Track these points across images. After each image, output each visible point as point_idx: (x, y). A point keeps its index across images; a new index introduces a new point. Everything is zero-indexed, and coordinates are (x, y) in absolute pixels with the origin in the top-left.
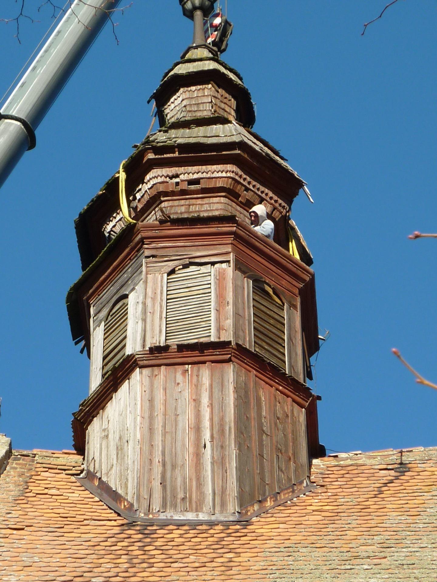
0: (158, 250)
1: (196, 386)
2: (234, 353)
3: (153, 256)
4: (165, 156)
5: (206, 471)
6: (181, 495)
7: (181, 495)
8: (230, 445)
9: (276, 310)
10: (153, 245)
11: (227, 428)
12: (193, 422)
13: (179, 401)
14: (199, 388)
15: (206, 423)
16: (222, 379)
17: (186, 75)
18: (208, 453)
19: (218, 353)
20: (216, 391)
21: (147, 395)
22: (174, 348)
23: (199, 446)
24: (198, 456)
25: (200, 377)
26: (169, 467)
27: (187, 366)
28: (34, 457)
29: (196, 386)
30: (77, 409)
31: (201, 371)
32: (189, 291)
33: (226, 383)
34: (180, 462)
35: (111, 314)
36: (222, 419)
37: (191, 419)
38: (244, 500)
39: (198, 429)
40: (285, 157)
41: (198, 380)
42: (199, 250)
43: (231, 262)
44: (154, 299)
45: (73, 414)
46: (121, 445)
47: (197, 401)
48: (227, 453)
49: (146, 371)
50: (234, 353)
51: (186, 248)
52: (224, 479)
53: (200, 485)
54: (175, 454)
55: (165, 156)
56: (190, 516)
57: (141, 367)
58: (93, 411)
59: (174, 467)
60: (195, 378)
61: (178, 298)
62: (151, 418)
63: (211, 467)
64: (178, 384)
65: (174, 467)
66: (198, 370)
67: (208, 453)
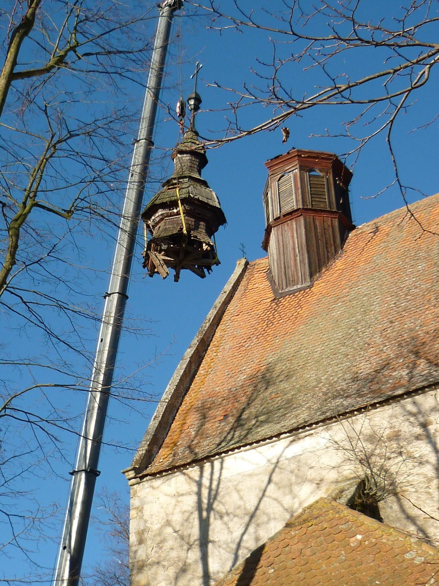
15: (297, 246)
18: (298, 258)
20: (299, 231)
23: (295, 256)
24: (295, 260)
36: (301, 242)
38: (311, 276)
47: (293, 236)
49: (275, 228)
65: (288, 268)
67: (298, 258)
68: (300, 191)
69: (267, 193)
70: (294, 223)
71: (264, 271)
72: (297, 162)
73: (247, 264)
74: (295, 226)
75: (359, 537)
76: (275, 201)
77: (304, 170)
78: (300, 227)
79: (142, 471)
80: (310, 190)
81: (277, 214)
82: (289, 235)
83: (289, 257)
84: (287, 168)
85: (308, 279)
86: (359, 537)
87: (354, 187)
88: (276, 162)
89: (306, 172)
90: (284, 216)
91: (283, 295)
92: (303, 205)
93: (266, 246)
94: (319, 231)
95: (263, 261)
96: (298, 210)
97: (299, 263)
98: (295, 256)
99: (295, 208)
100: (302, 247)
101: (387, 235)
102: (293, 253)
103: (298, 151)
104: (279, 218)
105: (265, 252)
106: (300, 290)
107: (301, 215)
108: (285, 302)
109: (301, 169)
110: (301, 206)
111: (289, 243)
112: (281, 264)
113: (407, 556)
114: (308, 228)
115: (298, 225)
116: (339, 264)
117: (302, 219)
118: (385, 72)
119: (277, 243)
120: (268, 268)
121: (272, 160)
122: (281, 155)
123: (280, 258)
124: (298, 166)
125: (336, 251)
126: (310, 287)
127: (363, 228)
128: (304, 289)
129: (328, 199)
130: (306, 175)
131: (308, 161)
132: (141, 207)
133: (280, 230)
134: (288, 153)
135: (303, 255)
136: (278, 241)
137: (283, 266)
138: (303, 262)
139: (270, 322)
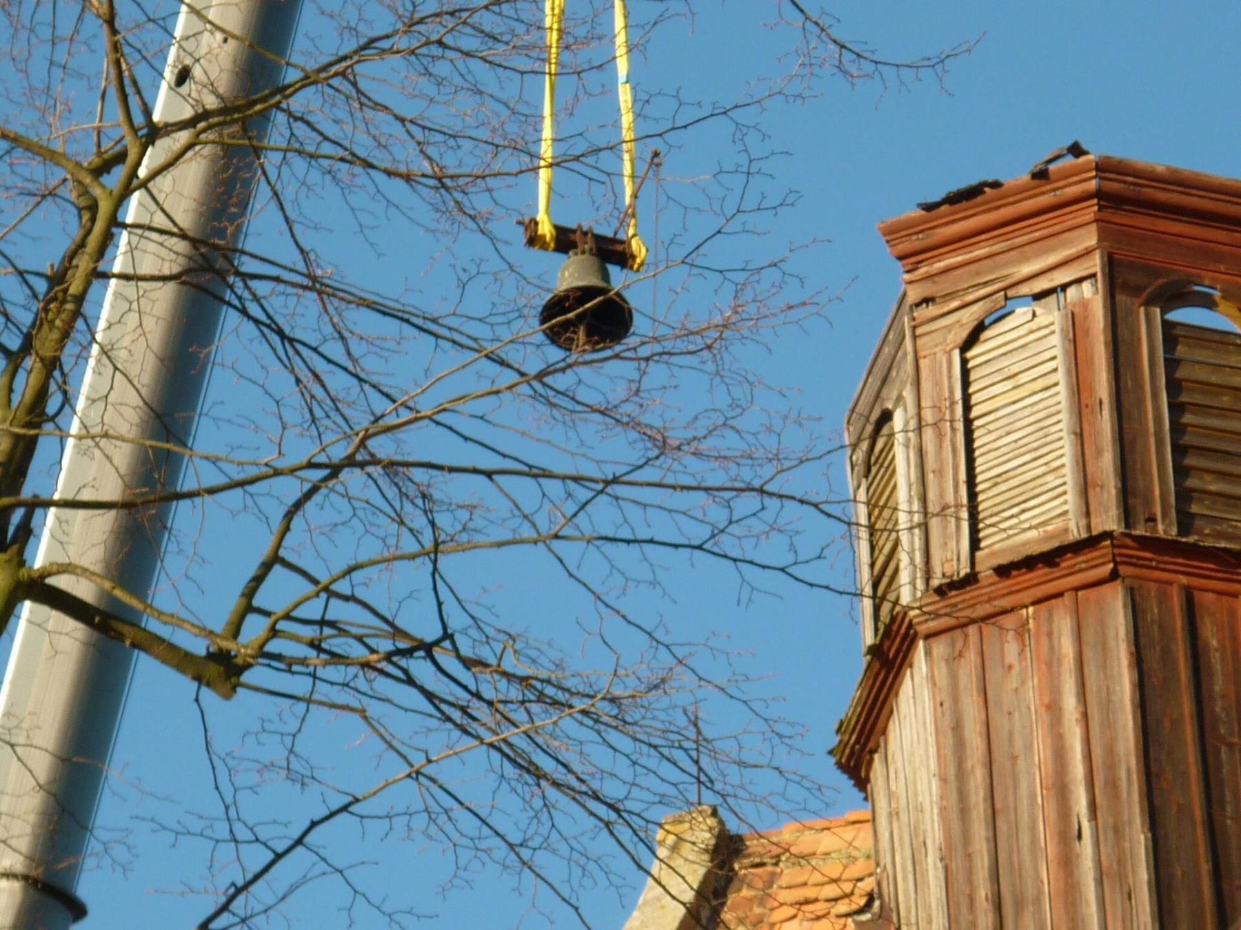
0: (936, 279)
1: (1049, 665)
2: (1121, 555)
3: (928, 300)
5: (1087, 903)
8: (1130, 823)
10: (923, 271)
11: (1123, 774)
12: (1050, 770)
13: (1016, 714)
14: (1055, 669)
15: (1078, 769)
16: (1104, 633)
18: (1086, 849)
19: (1083, 566)
20: (1091, 671)
21: (947, 714)
22: (987, 577)
23: (1067, 836)
24: (1068, 862)
25: (1055, 635)
26: (1008, 910)
27: (1024, 611)
28: (776, 864)
29: (1049, 665)
30: (834, 740)
31: (1056, 619)
32: (1014, 388)
33: (1111, 643)
34: (1030, 892)
35: (873, 459)
36: (1110, 751)
37: (1045, 763)
40: (716, 690)
41: (1052, 648)
42: (1026, 259)
43: (1099, 276)
45: (831, 752)
47: (1054, 708)
48: (1127, 845)
49: (940, 647)
50: (1121, 555)
51: (997, 258)
54: (1020, 869)
57: (928, 637)
58: (868, 740)
60: (1044, 641)
61: (997, 410)
63: (1097, 891)
64: (1010, 667)
65: (1019, 905)
66: (1050, 620)
67: (1086, 849)
68: (1105, 422)
69: (886, 416)
70: (1064, 626)
71: (843, 907)
72: (1090, 238)
73: (727, 849)
74: (1067, 647)
76: (940, 472)
77: (1135, 291)
78: (1104, 650)
81: (952, 556)
82: (1032, 696)
83: (1025, 839)
84: (1027, 269)
88: (960, 222)
89: (1148, 303)
90: (1003, 571)
92: (1128, 515)
93: (858, 752)
94: (1218, 687)
95: (827, 842)
96: (1090, 543)
98: (1067, 836)
99: (1076, 532)
100: (1113, 784)
102: (1052, 815)
103: (1104, 168)
104: (971, 579)
105: (845, 783)
107: (1114, 576)
109: (1119, 279)
110: (1108, 520)
111: (1029, 747)
112: (970, 881)
114: (1153, 658)
115: (1089, 637)
117: (1115, 602)
118: (872, 357)
119: (949, 741)
120: (868, 884)
121: (929, 207)
122: (996, 185)
123: (966, 840)
124: (1095, 264)
130: (1147, 327)
132: (700, 893)
133: (972, 656)
134: (1041, 175)
135: (1117, 831)
136: (957, 728)
137: (983, 891)
138: (1121, 877)
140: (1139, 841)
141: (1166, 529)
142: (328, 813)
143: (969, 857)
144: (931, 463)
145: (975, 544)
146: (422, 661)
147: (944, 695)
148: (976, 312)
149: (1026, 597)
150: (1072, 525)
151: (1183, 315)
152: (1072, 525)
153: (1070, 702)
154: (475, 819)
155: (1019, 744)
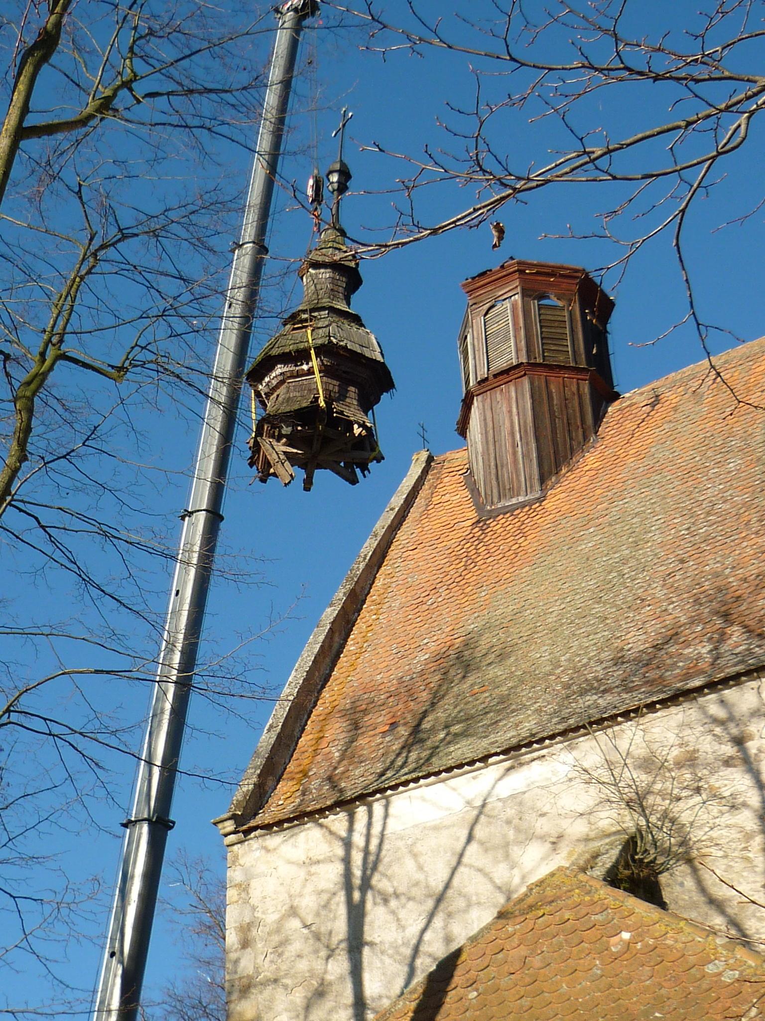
3: (475, 304)
4: (295, 451)
6: (508, 487)
7: (508, 487)
9: (558, 313)
15: (517, 428)
17: (441, 999)
20: (520, 402)
23: (514, 446)
24: (515, 453)
26: (499, 468)
34: (505, 462)
36: (525, 422)
38: (543, 480)
39: (512, 434)
44: (478, 339)
46: (477, 734)
47: (510, 412)
49: (480, 398)
52: (531, 467)
53: (518, 476)
55: (295, 451)
56: (514, 501)
57: (477, 395)
59: (502, 466)
62: (486, 433)
65: (502, 466)
68: (522, 332)
70: (513, 389)
72: (517, 283)
73: (430, 459)
74: (513, 394)
75: (626, 936)
76: (479, 350)
77: (530, 296)
78: (523, 395)
79: (248, 820)
80: (541, 332)
81: (483, 373)
83: (504, 449)
85: (537, 487)
86: (626, 936)
87: (616, 325)
89: (534, 299)
90: (495, 376)
91: (494, 515)
92: (529, 357)
93: (463, 428)
94: (555, 402)
95: (458, 455)
97: (522, 460)
100: (526, 431)
101: (675, 409)
102: (510, 441)
104: (487, 379)
106: (523, 505)
107: (525, 374)
108: (494, 526)
109: (525, 294)
112: (489, 461)
113: (710, 969)
114: (536, 397)
116: (590, 460)
117: (526, 382)
119: (483, 423)
120: (467, 466)
121: (473, 278)
122: (491, 270)
123: (488, 449)
125: (586, 438)
126: (541, 500)
127: (634, 397)
128: (530, 504)
129: (572, 347)
130: (534, 305)
131: (536, 281)
133: (489, 400)
134: (502, 267)
135: (527, 444)
136: (485, 420)
137: (493, 464)
138: (529, 456)
139: (470, 562)
140: (533, 446)
141: (540, 360)
142: (182, 766)
143: (489, 454)
144: (476, 349)
145: (488, 370)
146: (610, 38)
147: (481, 411)
148: (488, 306)
149: (502, 382)
150: (514, 361)
151: (543, 302)
152: (514, 361)
153: (514, 410)
154: (39, 110)
155: (501, 423)
